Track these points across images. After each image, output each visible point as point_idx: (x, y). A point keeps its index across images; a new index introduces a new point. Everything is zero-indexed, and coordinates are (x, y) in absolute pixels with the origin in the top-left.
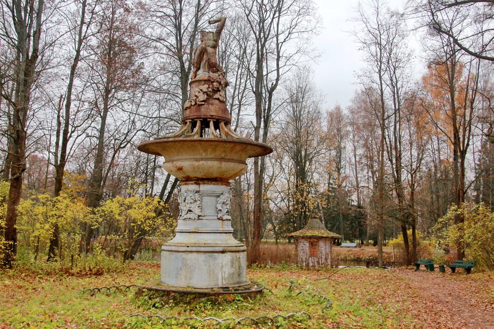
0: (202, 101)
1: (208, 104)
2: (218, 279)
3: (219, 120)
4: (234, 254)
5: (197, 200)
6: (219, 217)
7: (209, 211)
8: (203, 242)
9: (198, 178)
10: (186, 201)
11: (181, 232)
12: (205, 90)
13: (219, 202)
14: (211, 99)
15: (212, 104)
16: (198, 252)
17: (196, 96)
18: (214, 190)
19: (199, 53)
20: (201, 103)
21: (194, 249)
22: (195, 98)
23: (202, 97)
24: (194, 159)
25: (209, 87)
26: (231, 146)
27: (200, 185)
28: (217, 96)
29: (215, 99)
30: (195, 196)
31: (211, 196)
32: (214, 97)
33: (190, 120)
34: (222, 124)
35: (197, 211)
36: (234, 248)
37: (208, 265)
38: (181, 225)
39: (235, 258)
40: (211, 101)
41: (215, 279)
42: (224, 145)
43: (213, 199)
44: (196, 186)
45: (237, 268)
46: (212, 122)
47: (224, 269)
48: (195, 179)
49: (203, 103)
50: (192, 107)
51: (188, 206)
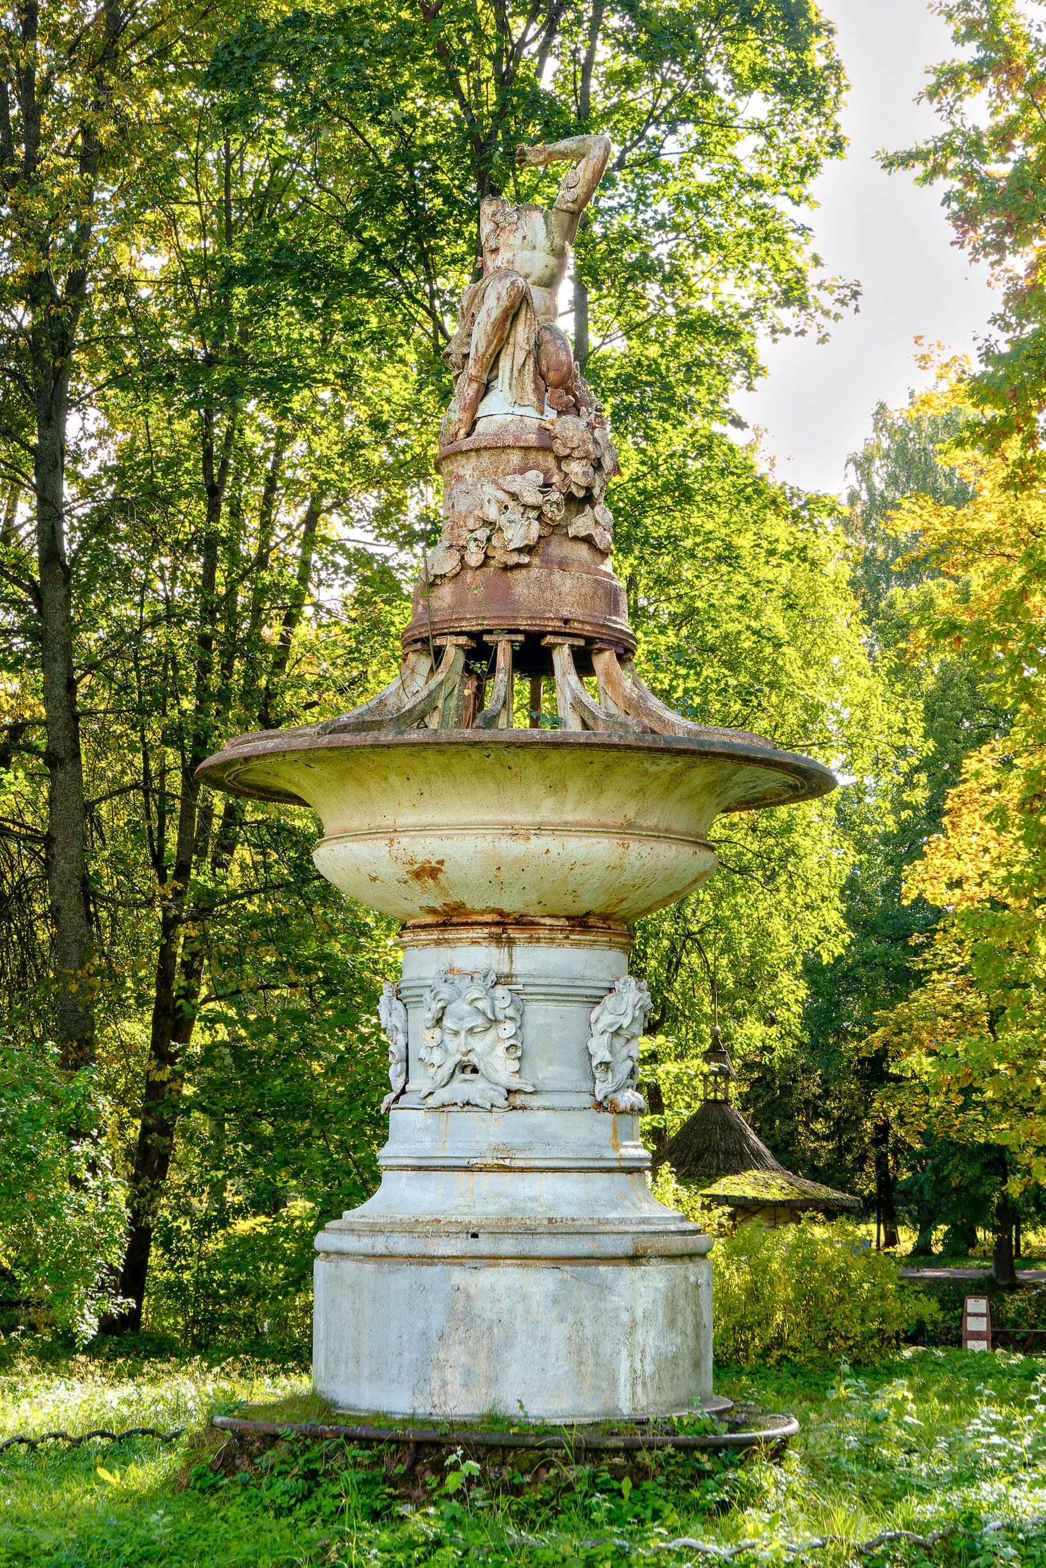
0: (519, 551)
1: (547, 563)
2: (614, 1383)
3: (544, 634)
4: (677, 1268)
5: (501, 1017)
6: (599, 1098)
7: (553, 1070)
8: (540, 1213)
9: (501, 913)
10: (447, 1022)
11: (420, 1168)
12: (532, 497)
13: (600, 1026)
14: (555, 539)
15: (563, 565)
16: (524, 1259)
17: (487, 523)
18: (578, 969)
19: (496, 313)
20: (515, 559)
21: (508, 1246)
22: (482, 534)
23: (520, 531)
24: (505, 826)
25: (547, 485)
26: (671, 769)
27: (517, 950)
28: (581, 525)
29: (575, 538)
30: (493, 999)
31: (564, 999)
32: (572, 531)
33: (462, 640)
34: (604, 661)
35: (502, 1068)
36: (679, 1238)
37: (570, 1318)
38: (410, 1134)
39: (683, 1287)
40: (558, 549)
41: (604, 1385)
42: (647, 765)
43: (574, 1011)
44: (494, 950)
45: (690, 1330)
46: (566, 650)
47: (640, 1335)
48: (488, 918)
49: (525, 559)
50: (469, 577)
51: (456, 1046)
